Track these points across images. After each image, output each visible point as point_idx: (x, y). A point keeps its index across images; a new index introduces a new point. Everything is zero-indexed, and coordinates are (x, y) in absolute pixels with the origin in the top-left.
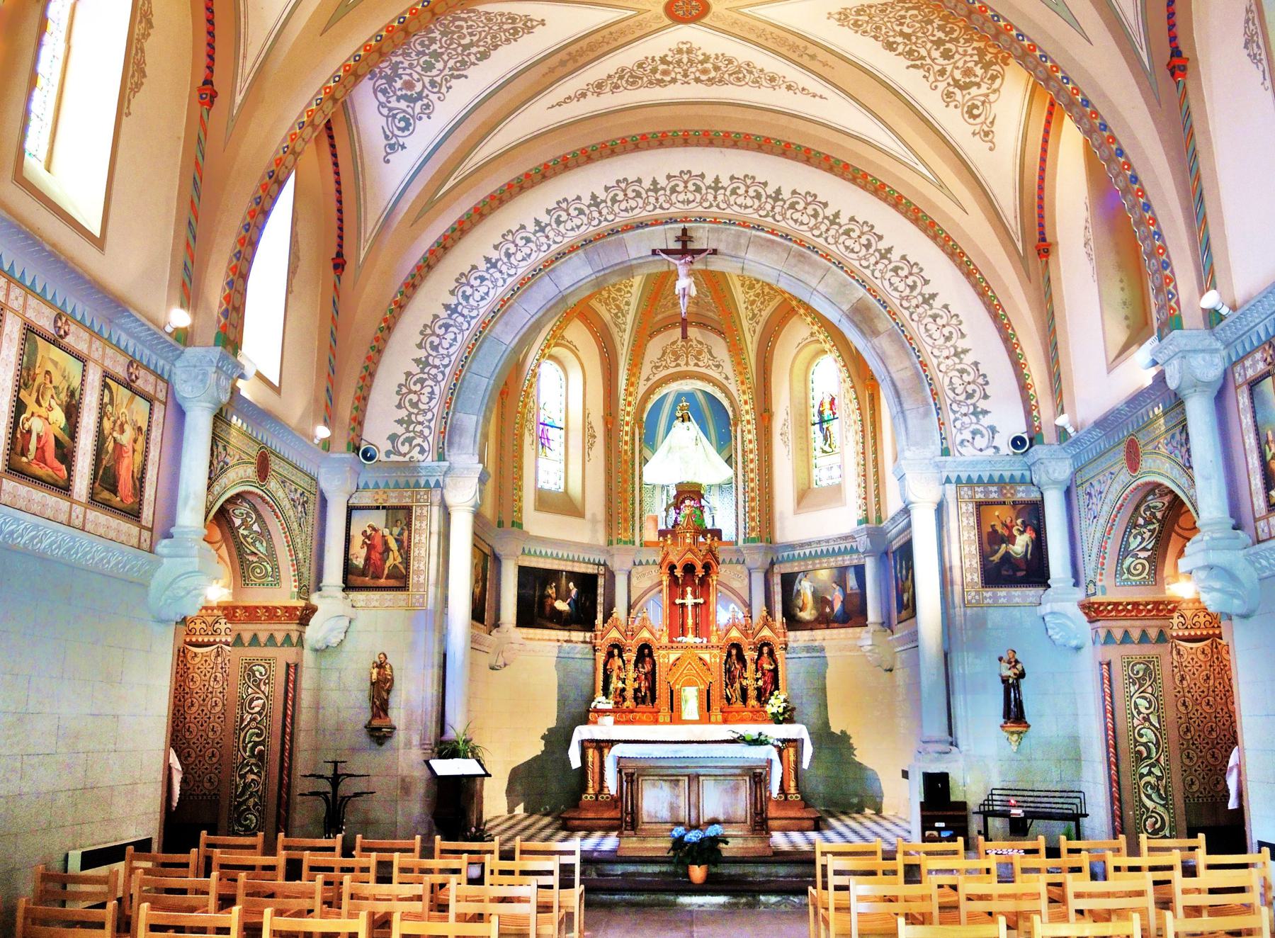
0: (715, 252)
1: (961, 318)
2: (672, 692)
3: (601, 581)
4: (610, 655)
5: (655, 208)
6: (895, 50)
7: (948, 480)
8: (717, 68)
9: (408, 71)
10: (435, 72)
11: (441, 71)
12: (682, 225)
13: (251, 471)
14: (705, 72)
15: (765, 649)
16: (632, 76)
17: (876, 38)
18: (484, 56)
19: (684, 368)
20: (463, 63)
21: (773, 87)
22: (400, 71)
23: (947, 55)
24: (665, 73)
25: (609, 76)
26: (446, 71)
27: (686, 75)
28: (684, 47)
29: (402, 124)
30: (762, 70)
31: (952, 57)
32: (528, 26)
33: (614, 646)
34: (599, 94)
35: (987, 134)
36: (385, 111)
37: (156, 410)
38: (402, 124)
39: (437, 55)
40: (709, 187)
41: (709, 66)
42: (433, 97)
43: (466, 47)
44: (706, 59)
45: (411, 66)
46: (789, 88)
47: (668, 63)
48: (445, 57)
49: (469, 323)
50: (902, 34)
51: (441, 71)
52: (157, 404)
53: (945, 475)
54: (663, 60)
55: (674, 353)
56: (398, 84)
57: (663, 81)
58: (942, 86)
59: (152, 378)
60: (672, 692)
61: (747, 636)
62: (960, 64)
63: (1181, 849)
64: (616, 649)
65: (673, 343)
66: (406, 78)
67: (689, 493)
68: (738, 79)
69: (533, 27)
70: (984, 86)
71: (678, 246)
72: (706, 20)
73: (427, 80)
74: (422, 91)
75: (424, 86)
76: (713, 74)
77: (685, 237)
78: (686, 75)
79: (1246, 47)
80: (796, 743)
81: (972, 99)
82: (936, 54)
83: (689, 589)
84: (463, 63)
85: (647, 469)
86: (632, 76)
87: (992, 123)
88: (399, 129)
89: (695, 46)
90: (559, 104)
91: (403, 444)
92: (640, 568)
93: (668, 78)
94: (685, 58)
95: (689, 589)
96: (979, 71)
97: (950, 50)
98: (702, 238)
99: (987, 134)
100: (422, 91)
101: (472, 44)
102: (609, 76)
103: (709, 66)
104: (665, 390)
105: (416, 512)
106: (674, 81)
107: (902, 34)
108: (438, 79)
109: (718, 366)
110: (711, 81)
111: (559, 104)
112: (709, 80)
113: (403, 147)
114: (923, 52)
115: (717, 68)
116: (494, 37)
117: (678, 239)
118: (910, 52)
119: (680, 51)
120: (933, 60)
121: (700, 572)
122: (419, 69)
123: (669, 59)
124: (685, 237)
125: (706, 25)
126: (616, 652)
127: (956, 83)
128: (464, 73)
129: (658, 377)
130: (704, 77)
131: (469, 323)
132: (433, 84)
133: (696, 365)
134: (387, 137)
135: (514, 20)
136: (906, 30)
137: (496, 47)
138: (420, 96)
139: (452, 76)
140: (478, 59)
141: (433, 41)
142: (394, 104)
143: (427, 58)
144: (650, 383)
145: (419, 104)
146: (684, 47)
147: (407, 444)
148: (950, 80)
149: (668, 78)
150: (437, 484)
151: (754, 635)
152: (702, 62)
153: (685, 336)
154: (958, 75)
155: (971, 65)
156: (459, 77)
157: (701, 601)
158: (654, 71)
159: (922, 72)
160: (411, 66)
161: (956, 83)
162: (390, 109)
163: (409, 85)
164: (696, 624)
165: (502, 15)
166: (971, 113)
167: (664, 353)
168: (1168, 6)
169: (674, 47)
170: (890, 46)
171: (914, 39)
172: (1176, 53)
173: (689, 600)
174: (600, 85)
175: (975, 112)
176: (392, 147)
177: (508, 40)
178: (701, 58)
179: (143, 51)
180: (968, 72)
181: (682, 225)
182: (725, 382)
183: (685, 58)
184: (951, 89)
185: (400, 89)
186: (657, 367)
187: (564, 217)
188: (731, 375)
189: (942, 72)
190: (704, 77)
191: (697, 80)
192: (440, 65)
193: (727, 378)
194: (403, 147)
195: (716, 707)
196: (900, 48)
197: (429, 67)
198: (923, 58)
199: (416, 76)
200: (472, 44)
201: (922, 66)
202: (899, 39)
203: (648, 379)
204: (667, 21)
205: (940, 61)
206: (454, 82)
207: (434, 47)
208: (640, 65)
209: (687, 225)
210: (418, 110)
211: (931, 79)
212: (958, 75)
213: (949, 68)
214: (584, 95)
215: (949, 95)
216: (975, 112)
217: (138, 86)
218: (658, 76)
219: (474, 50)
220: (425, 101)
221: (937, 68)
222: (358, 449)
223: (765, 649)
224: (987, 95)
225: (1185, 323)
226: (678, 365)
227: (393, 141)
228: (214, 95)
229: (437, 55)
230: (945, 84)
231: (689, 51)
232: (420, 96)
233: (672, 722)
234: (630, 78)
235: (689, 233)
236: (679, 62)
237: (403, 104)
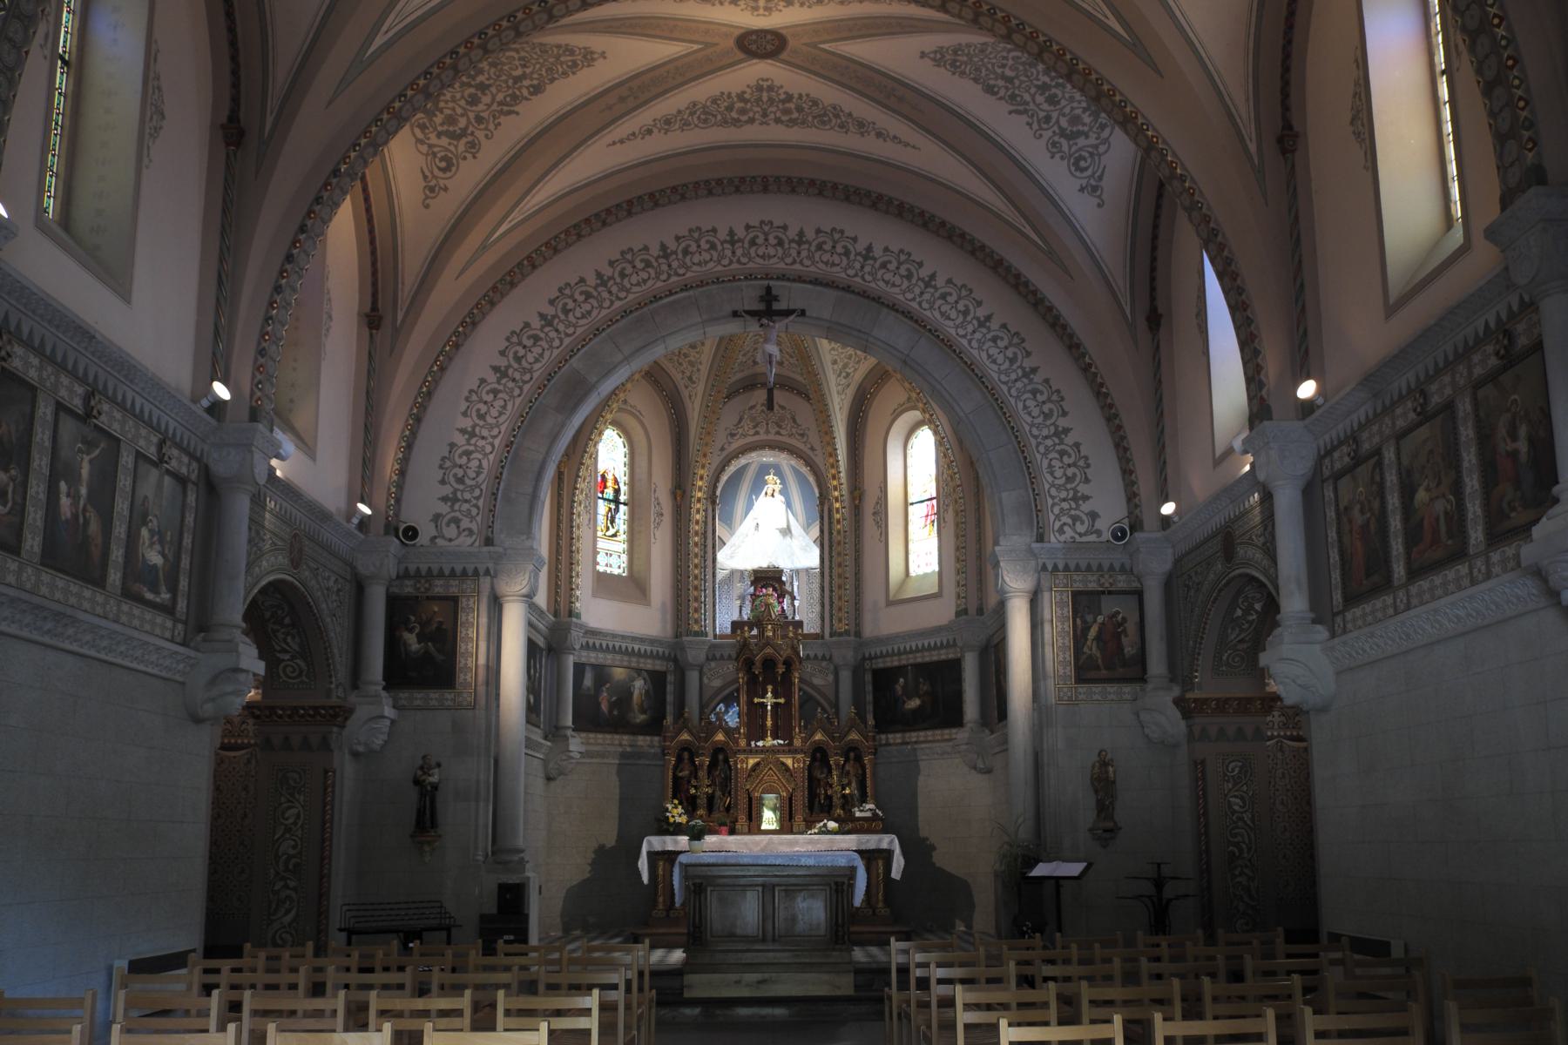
0: (803, 313)
1: (625, 248)
2: (750, 799)
3: (670, 678)
4: (680, 759)
5: (731, 262)
6: (995, 94)
7: (1044, 568)
8: (799, 109)
9: (451, 105)
10: (481, 107)
11: (489, 106)
12: (766, 283)
13: (282, 560)
14: (787, 112)
15: (852, 755)
16: (705, 113)
17: (976, 80)
18: (537, 90)
19: (762, 437)
20: (515, 98)
21: (862, 134)
22: (442, 105)
23: (1052, 100)
24: (743, 111)
25: (679, 112)
26: (495, 107)
27: (765, 115)
28: (765, 84)
29: (443, 164)
30: (850, 115)
31: (1058, 102)
32: (589, 57)
33: (684, 749)
34: (667, 131)
35: (1095, 189)
36: (424, 149)
37: (1422, 429)
38: (443, 164)
39: (483, 87)
40: (792, 241)
41: (792, 106)
42: (480, 135)
43: (517, 80)
44: (789, 98)
45: (454, 100)
46: (879, 135)
47: (746, 101)
48: (493, 90)
49: (521, 388)
50: (1003, 77)
51: (489, 106)
52: (190, 486)
53: (1040, 562)
54: (741, 97)
55: (753, 419)
56: (439, 119)
57: (738, 120)
58: (1047, 134)
59: (185, 459)
60: (750, 799)
61: (833, 739)
62: (1067, 110)
63: (1302, 973)
64: (687, 753)
65: (752, 408)
66: (448, 112)
67: (768, 579)
68: (824, 123)
69: (593, 60)
70: (1093, 136)
71: (762, 307)
72: (784, 56)
73: (472, 115)
74: (466, 128)
75: (469, 122)
76: (795, 115)
77: (769, 296)
78: (765, 115)
79: (1352, 123)
80: (887, 855)
81: (1080, 149)
82: (1040, 99)
83: (770, 688)
84: (515, 98)
85: (720, 556)
86: (705, 113)
87: (1101, 178)
88: (440, 169)
89: (777, 83)
90: (622, 142)
91: (448, 525)
92: (713, 664)
93: (744, 118)
94: (765, 96)
95: (770, 688)
96: (1087, 119)
97: (1055, 95)
98: (790, 295)
99: (1095, 189)
100: (466, 128)
101: (524, 76)
102: (679, 112)
103: (792, 106)
104: (743, 461)
105: (463, 602)
106: (752, 121)
107: (1003, 77)
108: (484, 115)
109: (802, 435)
110: (793, 122)
111: (622, 142)
112: (791, 120)
113: (446, 189)
114: (1027, 97)
115: (799, 109)
116: (550, 70)
117: (762, 299)
118: (1013, 97)
119: (760, 88)
120: (1038, 105)
121: (781, 669)
122: (463, 103)
123: (747, 96)
124: (769, 296)
125: (783, 62)
126: (686, 755)
127: (1063, 133)
128: (515, 109)
129: (735, 445)
130: (784, 118)
131: (521, 388)
132: (479, 119)
133: (778, 433)
134: (425, 177)
135: (572, 52)
136: (1008, 73)
137: (552, 80)
138: (464, 133)
139: (501, 112)
140: (531, 94)
141: (481, 72)
142: (433, 140)
143: (472, 90)
144: (725, 453)
145: (464, 140)
146: (765, 84)
147: (453, 526)
148: (1056, 128)
149: (744, 118)
150: (487, 572)
151: (841, 738)
152: (783, 102)
153: (770, 404)
154: (1064, 123)
155: (1078, 111)
156: (510, 113)
157: (782, 701)
158: (730, 108)
159: (1025, 118)
160: (454, 100)
161: (1063, 133)
162: (430, 146)
163: (451, 120)
164: (775, 725)
165: (559, 46)
166: (1077, 165)
167: (741, 420)
168: (1289, 5)
169: (753, 83)
170: (990, 90)
171: (1017, 82)
172: (1288, 126)
173: (769, 700)
174: (668, 122)
175: (1083, 164)
176: (432, 189)
177: (565, 74)
178: (783, 97)
179: (159, 89)
180: (1075, 120)
181: (766, 283)
182: (810, 453)
183: (765, 96)
184: (1056, 138)
185: (442, 124)
186: (733, 435)
187: (629, 270)
188: (817, 446)
189: (1048, 119)
190: (784, 118)
191: (778, 121)
192: (486, 99)
193: (812, 449)
194: (446, 189)
195: (799, 818)
196: (1002, 93)
197: (474, 101)
198: (1027, 103)
199: (459, 111)
200: (524, 76)
201: (1026, 111)
202: (1001, 83)
203: (722, 449)
204: (742, 56)
205: (1045, 106)
206: (502, 119)
207: (481, 78)
208: (714, 101)
209: (772, 283)
210: (461, 148)
211: (1035, 126)
212: (1064, 123)
213: (1055, 115)
214: (650, 132)
215: (1054, 144)
216: (1083, 164)
217: (157, 129)
218: (734, 115)
219: (526, 83)
220: (470, 138)
221: (1042, 114)
222: (397, 530)
223: (852, 755)
224: (1096, 147)
225: (1146, 527)
226: (757, 433)
227: (433, 183)
228: (241, 133)
229: (483, 87)
230: (1050, 133)
231: (770, 88)
232: (464, 133)
233: (750, 832)
234: (703, 114)
235: (774, 292)
236: (759, 100)
237: (444, 141)
